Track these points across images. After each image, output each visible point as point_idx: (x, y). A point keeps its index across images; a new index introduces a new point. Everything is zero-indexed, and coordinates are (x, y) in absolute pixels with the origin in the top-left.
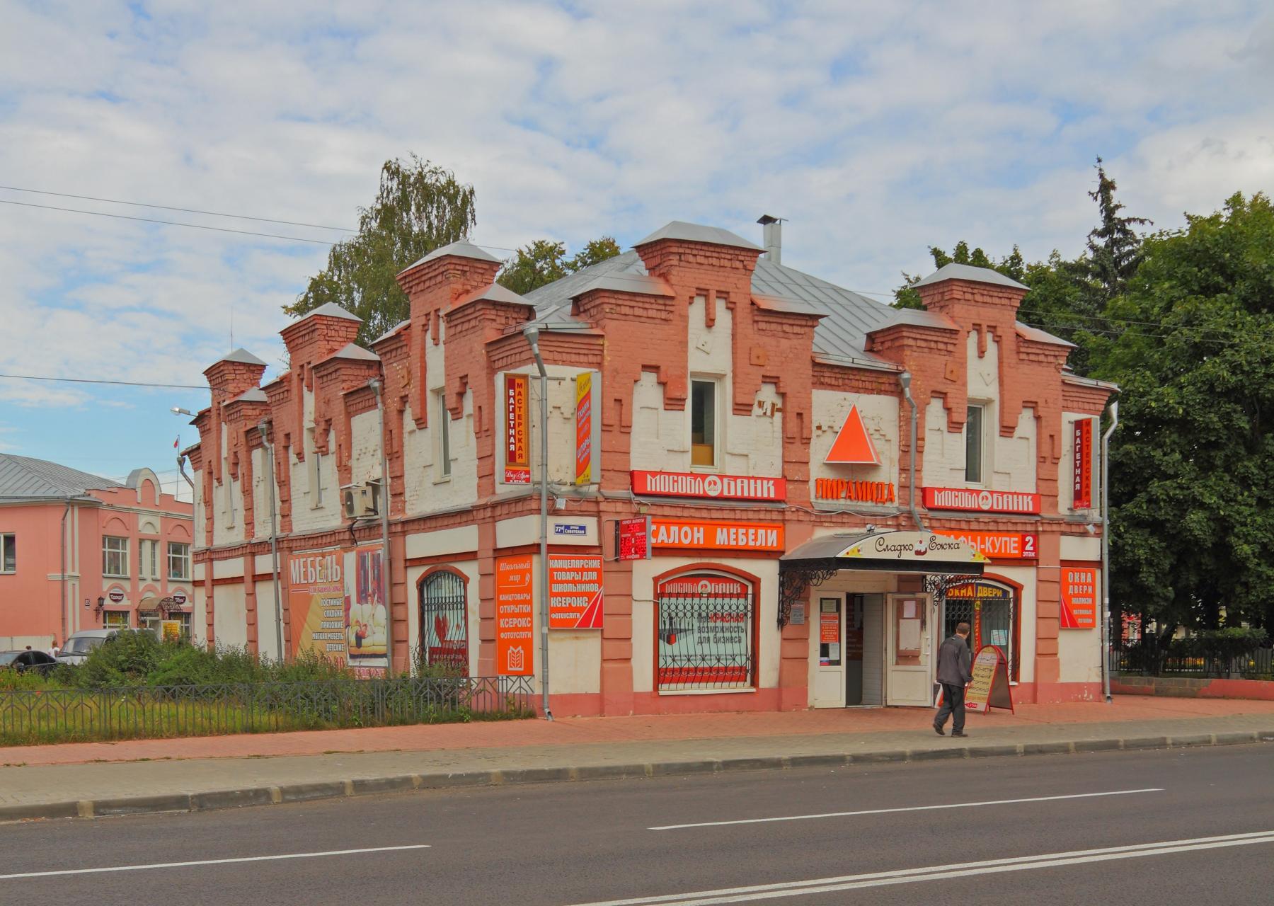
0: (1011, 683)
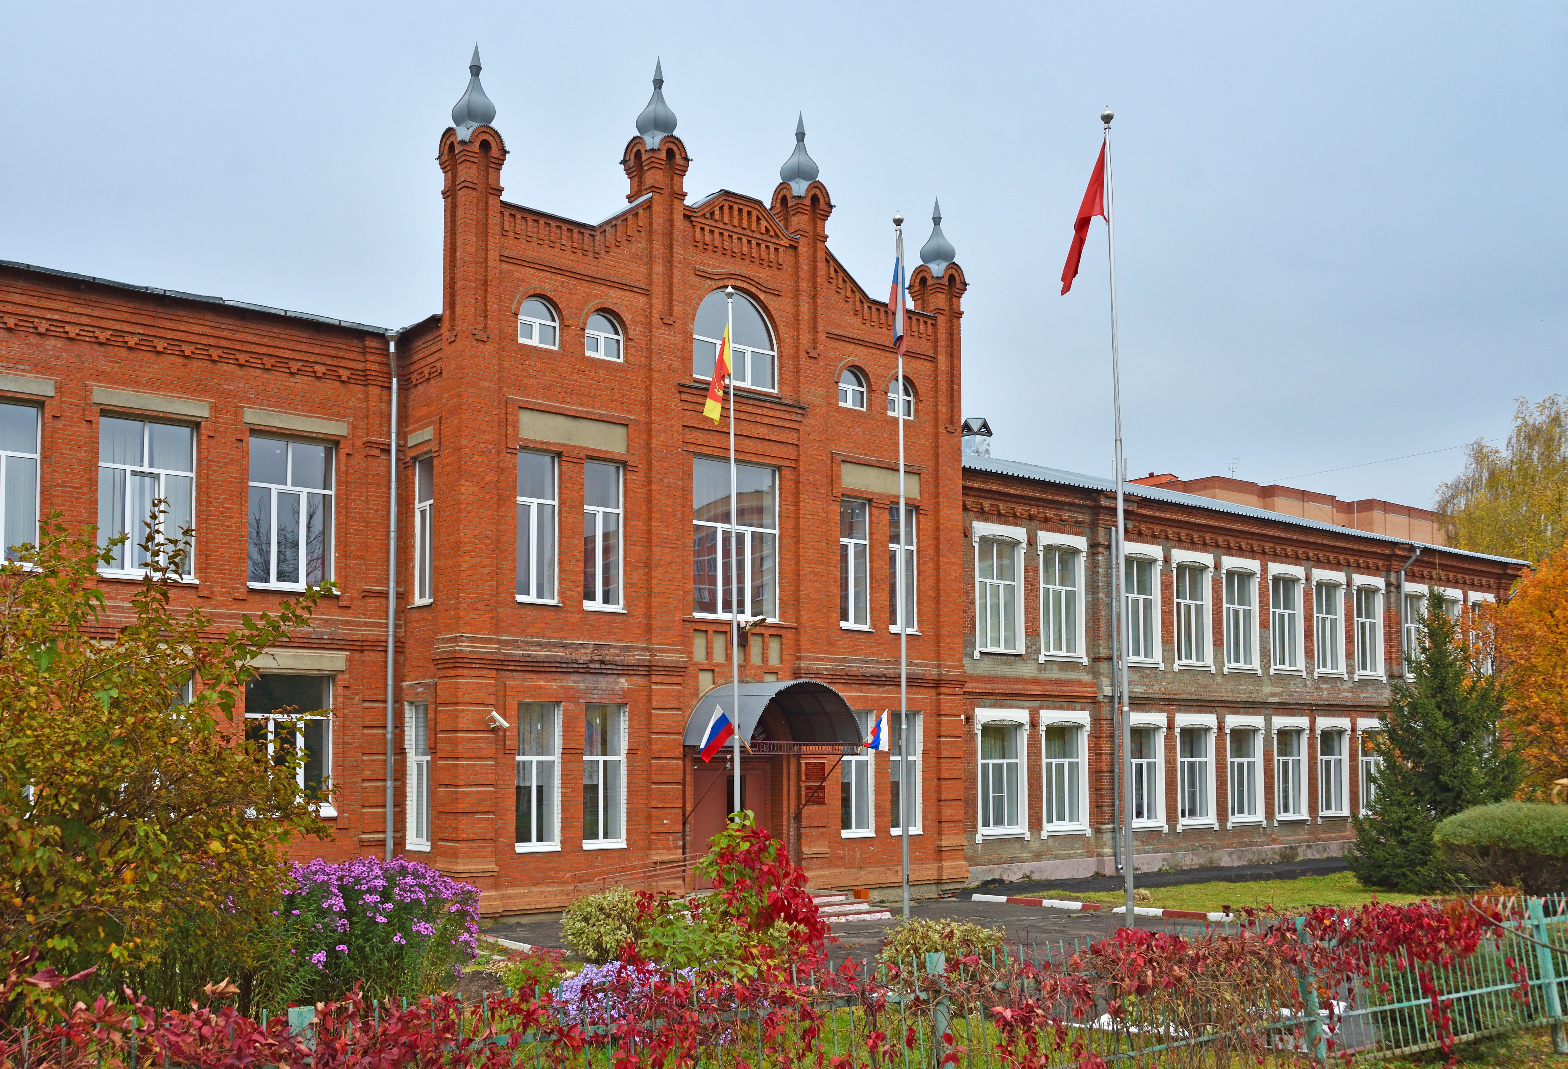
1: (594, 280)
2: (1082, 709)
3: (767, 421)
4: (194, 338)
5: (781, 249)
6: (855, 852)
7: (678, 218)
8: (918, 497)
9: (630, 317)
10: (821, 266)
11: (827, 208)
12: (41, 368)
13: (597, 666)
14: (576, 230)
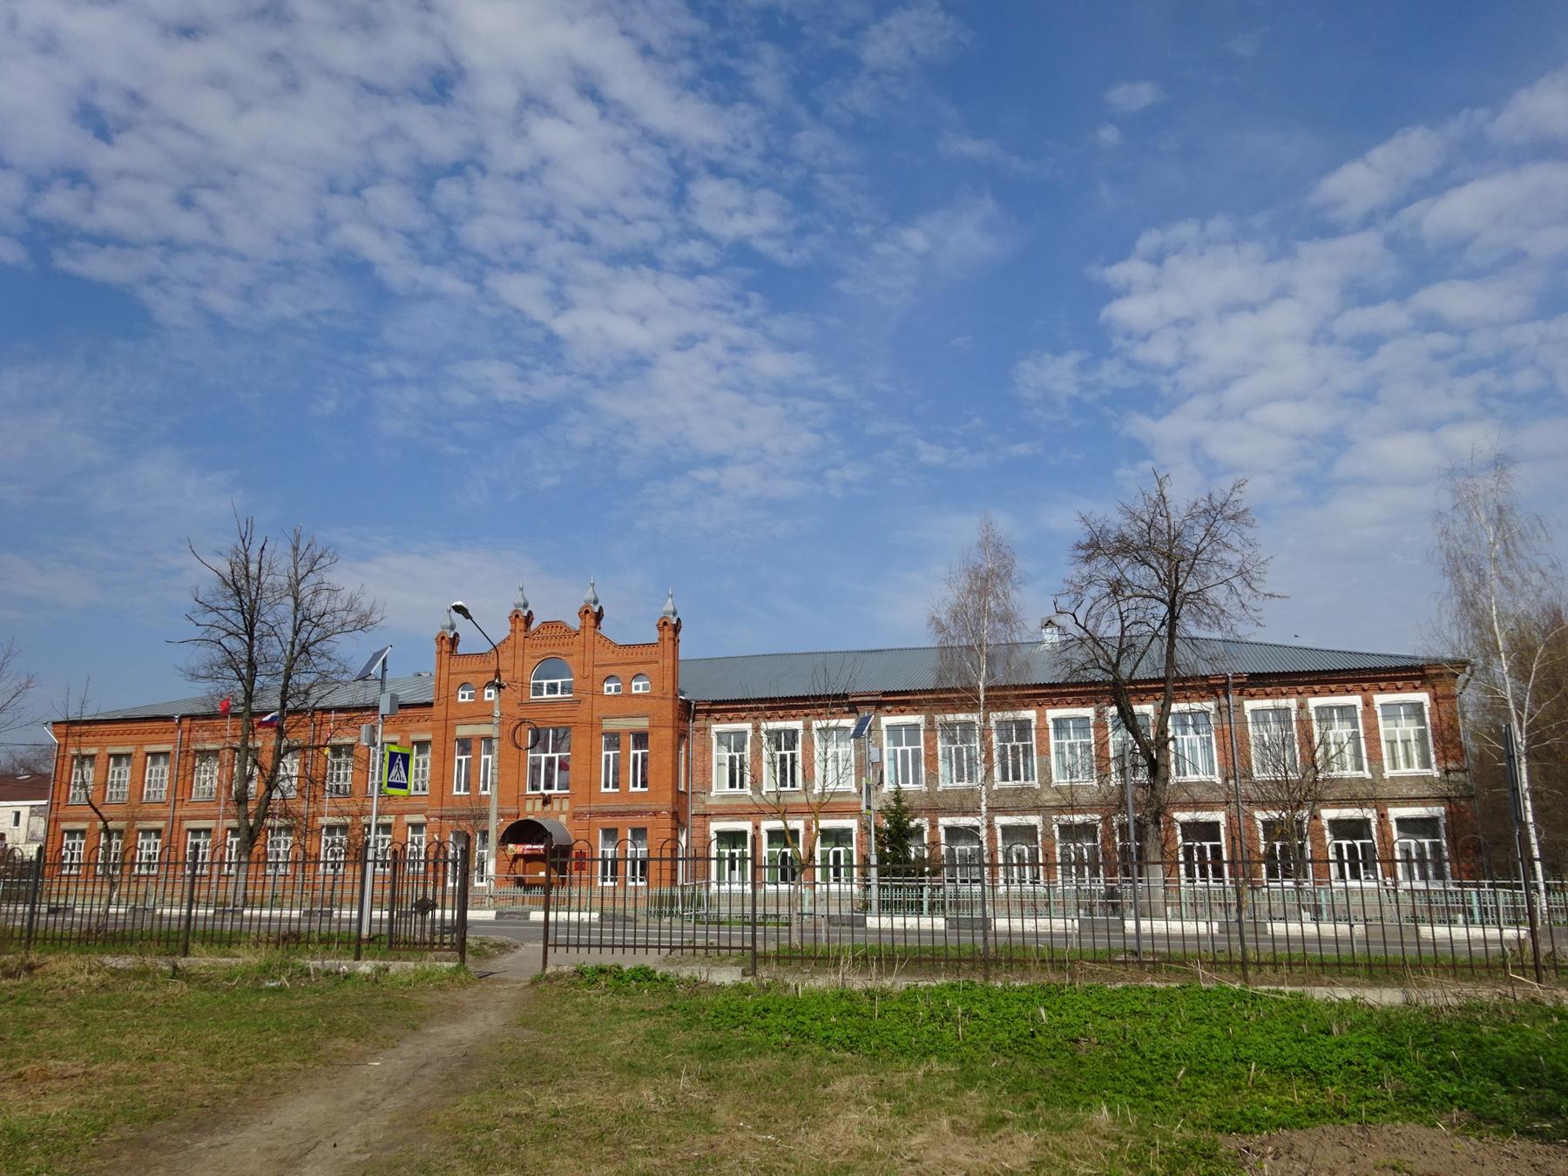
2: (539, 910)
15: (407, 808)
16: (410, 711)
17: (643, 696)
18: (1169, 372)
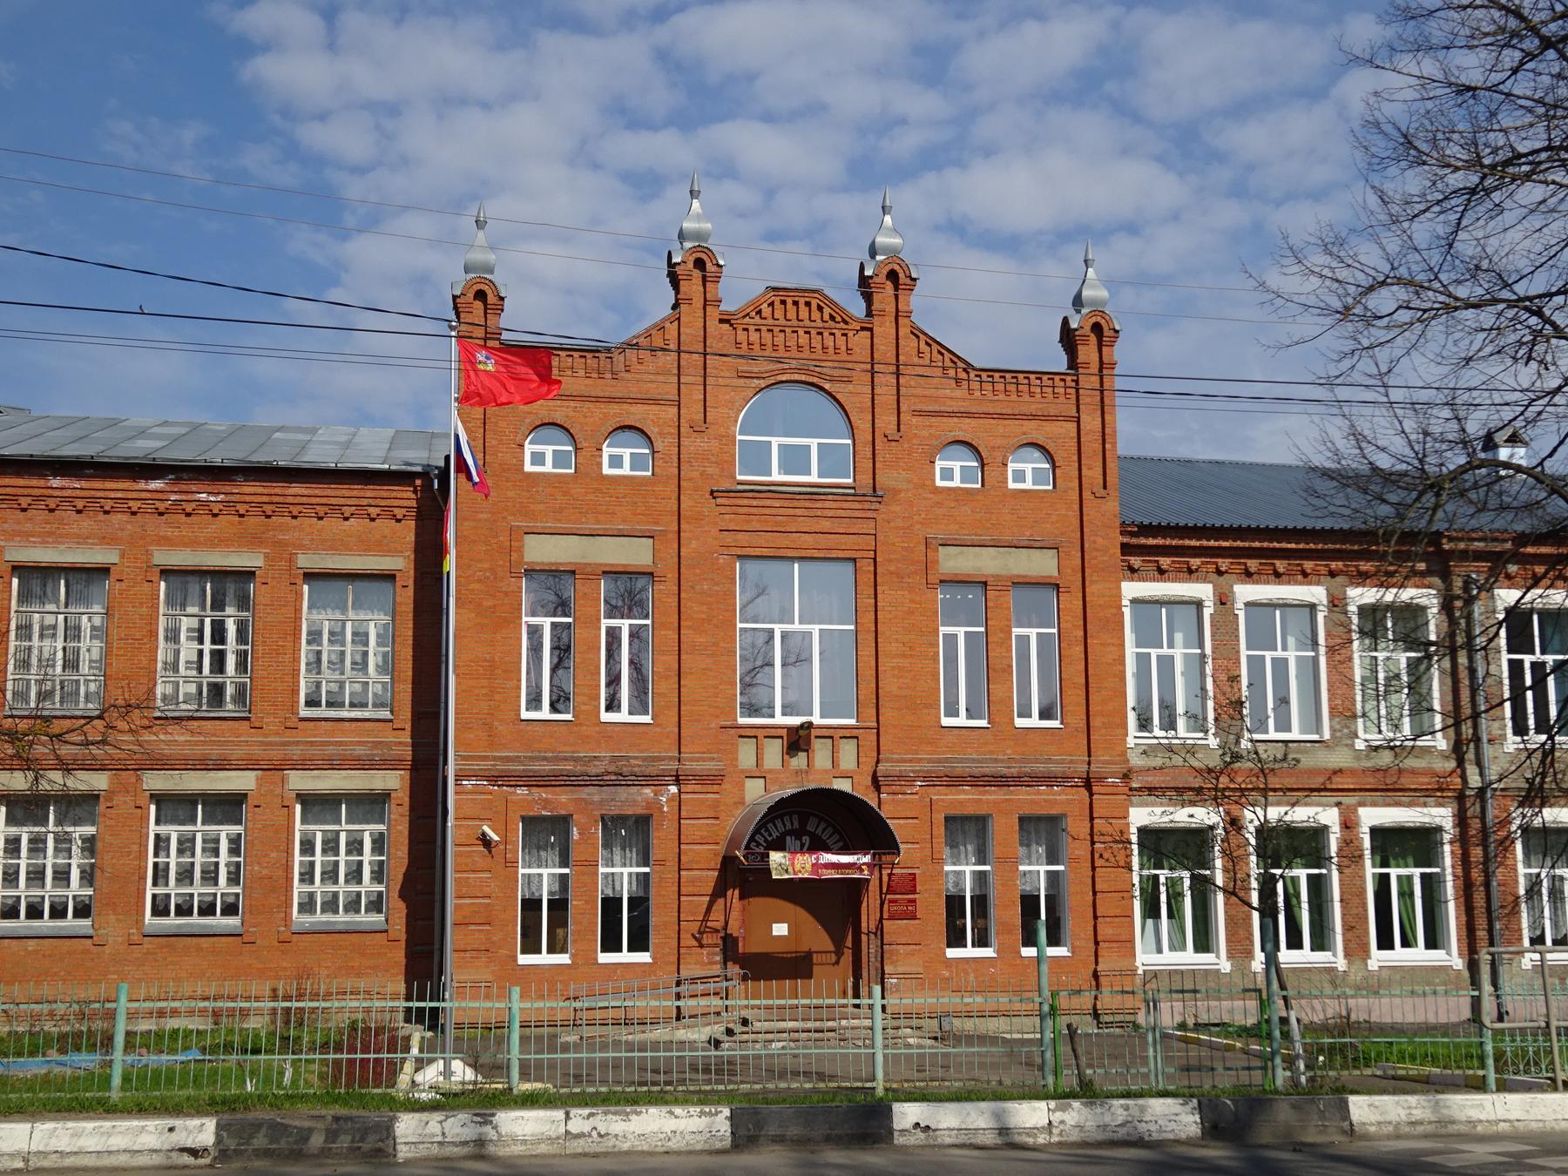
0: (606, 717)
1: (612, 400)
3: (830, 513)
4: (248, 499)
5: (851, 334)
6: (967, 973)
7: (713, 324)
8: (1056, 574)
9: (656, 430)
10: (909, 344)
11: (908, 281)
12: (106, 540)
13: (613, 778)
14: (589, 355)
15: (296, 752)
16: (297, 489)
17: (813, 493)
18: (358, 170)
